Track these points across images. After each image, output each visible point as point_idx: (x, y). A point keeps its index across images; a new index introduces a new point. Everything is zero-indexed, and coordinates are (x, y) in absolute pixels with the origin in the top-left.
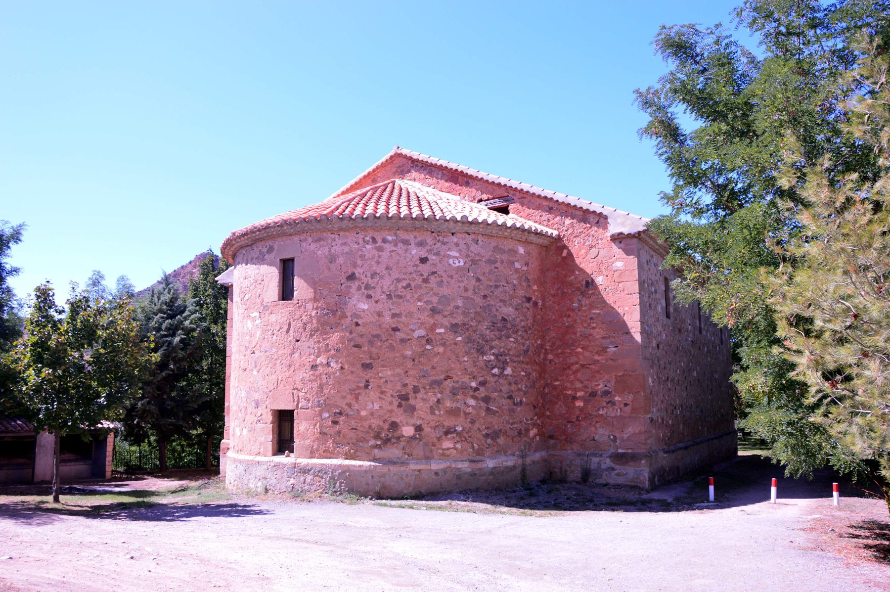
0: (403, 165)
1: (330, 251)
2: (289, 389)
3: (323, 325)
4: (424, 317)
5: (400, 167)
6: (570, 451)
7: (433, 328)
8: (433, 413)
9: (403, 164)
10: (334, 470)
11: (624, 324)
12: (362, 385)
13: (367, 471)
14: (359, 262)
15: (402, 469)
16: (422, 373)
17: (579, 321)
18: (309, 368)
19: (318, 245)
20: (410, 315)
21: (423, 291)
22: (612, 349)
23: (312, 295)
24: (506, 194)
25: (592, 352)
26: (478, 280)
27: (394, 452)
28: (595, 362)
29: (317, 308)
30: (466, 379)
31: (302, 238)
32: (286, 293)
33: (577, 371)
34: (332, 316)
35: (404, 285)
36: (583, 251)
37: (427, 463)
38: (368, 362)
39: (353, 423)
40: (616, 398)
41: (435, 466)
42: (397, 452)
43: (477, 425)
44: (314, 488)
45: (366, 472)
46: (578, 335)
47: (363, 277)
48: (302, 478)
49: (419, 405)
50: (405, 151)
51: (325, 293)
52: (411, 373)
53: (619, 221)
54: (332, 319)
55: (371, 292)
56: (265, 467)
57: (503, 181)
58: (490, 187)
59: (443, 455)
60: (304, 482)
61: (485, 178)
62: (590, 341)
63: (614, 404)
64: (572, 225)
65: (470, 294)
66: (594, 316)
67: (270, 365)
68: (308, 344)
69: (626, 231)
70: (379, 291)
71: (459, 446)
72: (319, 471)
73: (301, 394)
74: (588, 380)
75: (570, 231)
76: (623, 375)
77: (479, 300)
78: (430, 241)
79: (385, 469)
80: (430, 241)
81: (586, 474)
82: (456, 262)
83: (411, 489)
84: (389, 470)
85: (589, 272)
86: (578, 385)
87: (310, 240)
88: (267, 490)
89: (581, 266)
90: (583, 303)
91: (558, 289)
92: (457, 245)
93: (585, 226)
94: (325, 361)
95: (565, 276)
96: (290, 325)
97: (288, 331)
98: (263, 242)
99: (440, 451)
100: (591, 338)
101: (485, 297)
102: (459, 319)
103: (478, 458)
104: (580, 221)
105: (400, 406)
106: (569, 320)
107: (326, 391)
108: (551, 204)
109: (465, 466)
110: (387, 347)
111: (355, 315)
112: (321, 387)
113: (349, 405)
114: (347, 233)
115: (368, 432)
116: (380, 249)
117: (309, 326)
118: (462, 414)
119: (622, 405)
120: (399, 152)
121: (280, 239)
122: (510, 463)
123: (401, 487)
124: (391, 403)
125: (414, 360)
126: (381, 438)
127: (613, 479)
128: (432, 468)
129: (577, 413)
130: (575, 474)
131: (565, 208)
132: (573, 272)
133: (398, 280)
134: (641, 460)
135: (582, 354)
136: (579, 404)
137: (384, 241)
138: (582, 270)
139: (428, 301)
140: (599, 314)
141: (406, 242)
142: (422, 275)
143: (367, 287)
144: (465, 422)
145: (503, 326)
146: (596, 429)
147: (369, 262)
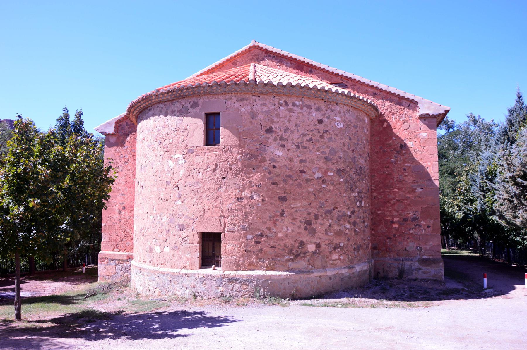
0: (258, 55)
1: (252, 109)
2: (216, 216)
3: (246, 166)
4: (321, 163)
5: (256, 55)
6: (388, 258)
7: (326, 172)
8: (327, 234)
9: (258, 54)
10: (258, 279)
11: (428, 174)
12: (279, 213)
13: (285, 279)
14: (275, 119)
15: (309, 276)
16: (320, 205)
17: (395, 170)
18: (235, 200)
19: (241, 103)
20: (312, 161)
21: (320, 144)
22: (419, 190)
23: (237, 143)
24: (341, 82)
25: (405, 192)
26: (350, 139)
27: (302, 264)
28: (407, 199)
29: (241, 153)
30: (345, 210)
31: (227, 97)
32: (211, 138)
33: (394, 204)
34: (253, 159)
35: (308, 139)
36: (399, 124)
37: (324, 271)
38: (283, 195)
39: (272, 243)
40: (422, 223)
41: (330, 273)
42: (304, 263)
43: (351, 242)
44: (241, 294)
45: (284, 279)
46: (395, 180)
47: (278, 131)
48: (230, 287)
49: (319, 228)
50: (261, 45)
51: (248, 141)
52: (314, 204)
53: (426, 106)
54: (254, 162)
55: (284, 143)
56: (194, 278)
57: (340, 72)
58: (329, 75)
59: (333, 264)
60: (232, 290)
61: (327, 69)
62: (403, 184)
63: (420, 226)
64: (390, 106)
65: (346, 148)
66: (407, 168)
67: (196, 197)
68: (231, 180)
69: (431, 113)
70: (290, 142)
71: (341, 257)
72: (246, 281)
73: (227, 220)
74: (402, 210)
75: (389, 110)
76: (427, 207)
77: (350, 153)
78: (324, 108)
79: (298, 277)
80: (324, 108)
81: (402, 273)
82: (339, 124)
83: (315, 290)
84: (300, 277)
85: (403, 138)
86: (395, 214)
87: (234, 99)
88: (195, 296)
89: (397, 134)
90: (399, 159)
91: (380, 149)
92: (339, 112)
93: (400, 107)
94: (249, 195)
95: (386, 140)
96: (216, 165)
97: (215, 170)
98: (186, 99)
99: (331, 262)
100: (404, 182)
101: (353, 151)
102: (341, 166)
103: (352, 265)
104: (396, 104)
105: (306, 229)
106: (389, 169)
107: (250, 218)
108: (375, 91)
109: (345, 271)
110: (297, 185)
111: (272, 160)
112: (246, 215)
113: (269, 229)
114: (265, 97)
115: (284, 250)
116: (291, 111)
117: (234, 167)
118: (343, 235)
119: (426, 227)
120: (256, 44)
121: (205, 97)
122: (365, 268)
123: (308, 290)
124: (300, 227)
125: (315, 195)
126: (293, 254)
127: (420, 275)
128: (328, 274)
129: (394, 232)
130: (394, 273)
131: (385, 94)
132: (391, 138)
133: (304, 135)
134: (440, 262)
135: (398, 193)
136: (396, 226)
137: (294, 105)
138: (397, 137)
139: (323, 152)
140: (410, 167)
141: (309, 107)
142: (319, 132)
143: (282, 139)
144: (345, 240)
145: (359, 171)
146: (407, 242)
147: (283, 120)
